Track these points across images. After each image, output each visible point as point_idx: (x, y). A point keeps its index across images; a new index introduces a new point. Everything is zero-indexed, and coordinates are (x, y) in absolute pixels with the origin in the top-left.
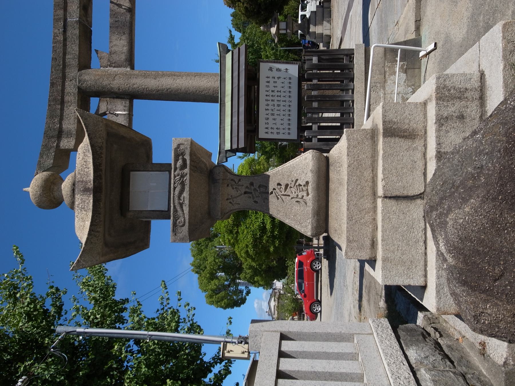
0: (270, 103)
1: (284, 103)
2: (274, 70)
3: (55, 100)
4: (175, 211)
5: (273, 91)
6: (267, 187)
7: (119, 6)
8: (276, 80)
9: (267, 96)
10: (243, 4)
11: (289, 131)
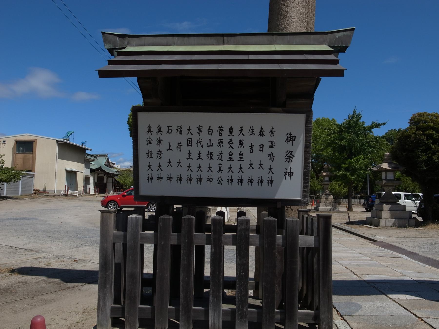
0: (215, 137)
1: (215, 168)
2: (289, 146)
5: (241, 143)
8: (267, 150)
9: (231, 129)
10: (414, 133)
11: (155, 179)
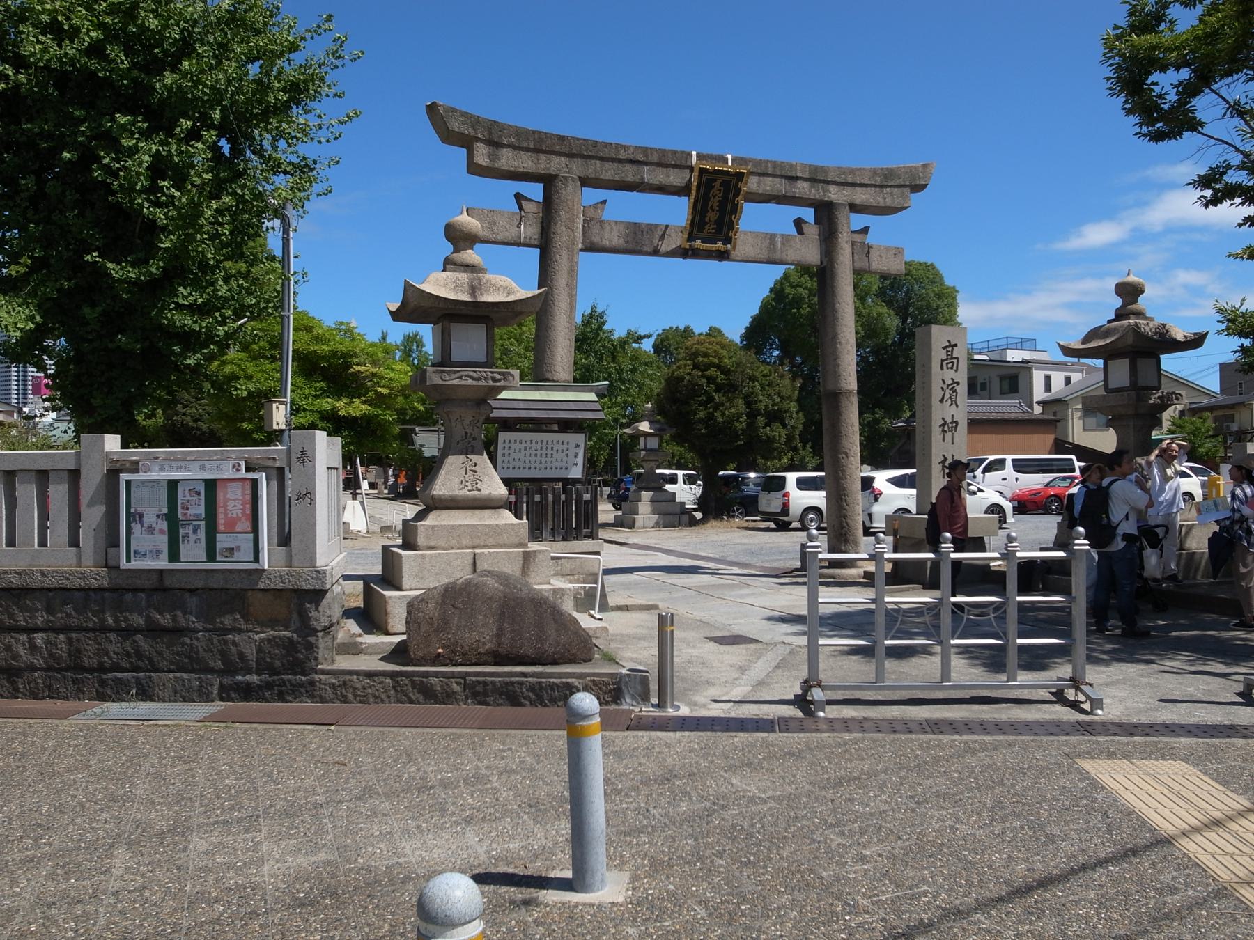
0: (539, 446)
3: (541, 140)
4: (455, 372)
6: (472, 453)
7: (662, 238)
